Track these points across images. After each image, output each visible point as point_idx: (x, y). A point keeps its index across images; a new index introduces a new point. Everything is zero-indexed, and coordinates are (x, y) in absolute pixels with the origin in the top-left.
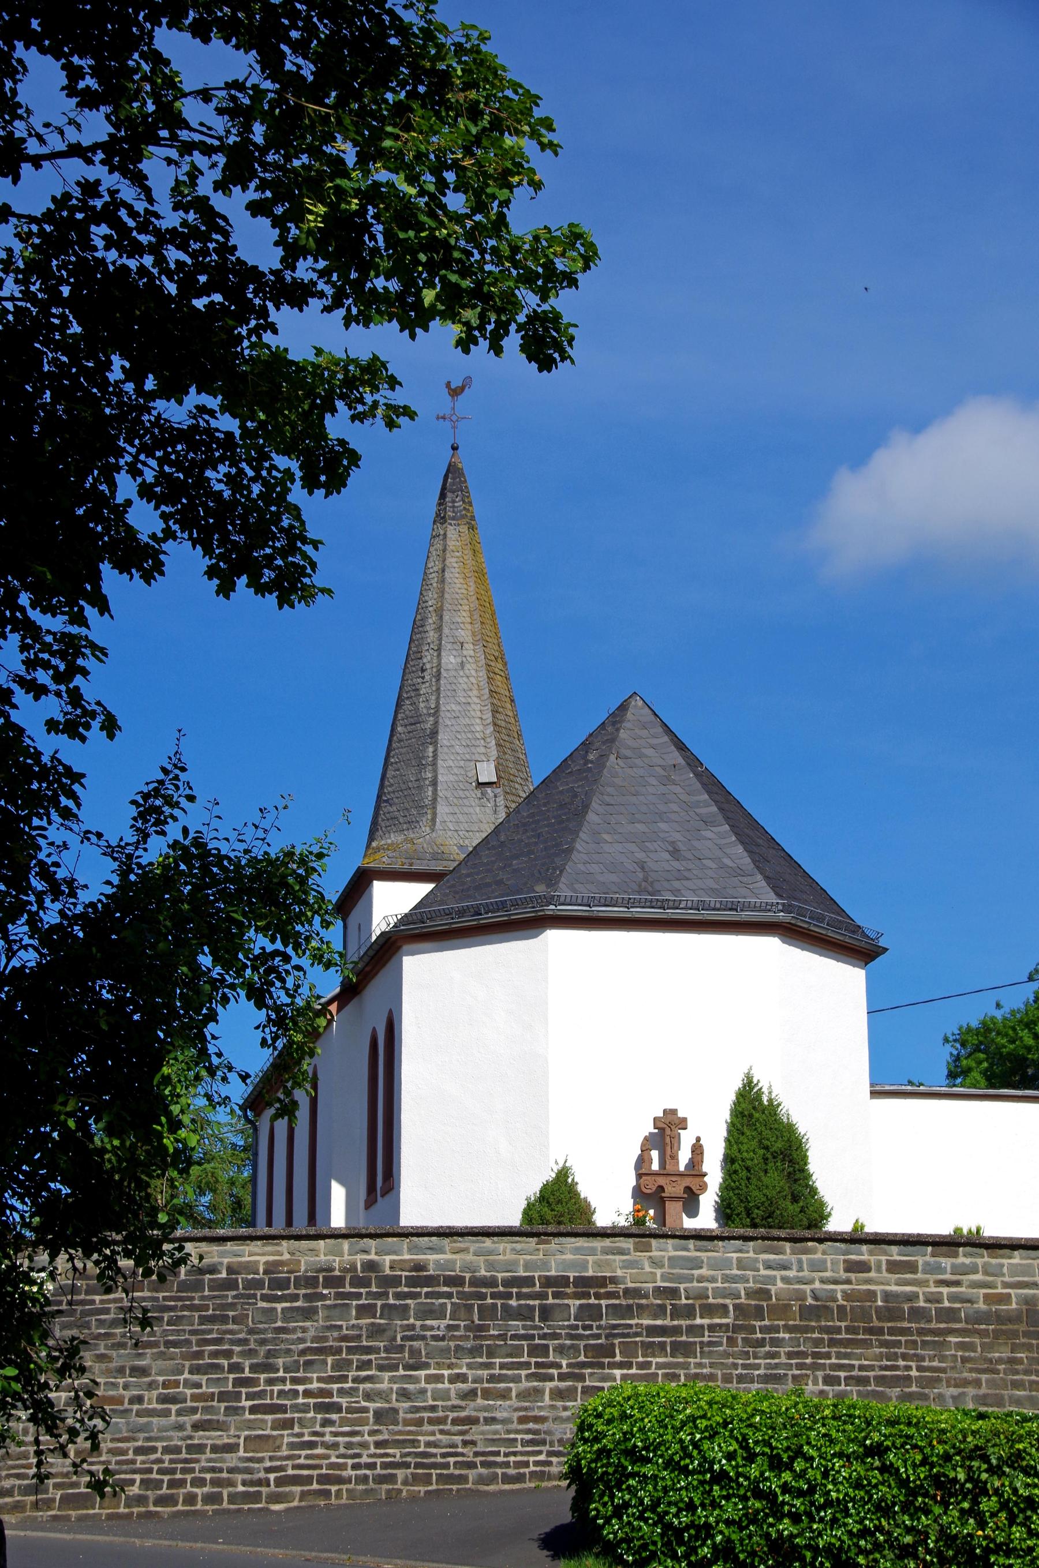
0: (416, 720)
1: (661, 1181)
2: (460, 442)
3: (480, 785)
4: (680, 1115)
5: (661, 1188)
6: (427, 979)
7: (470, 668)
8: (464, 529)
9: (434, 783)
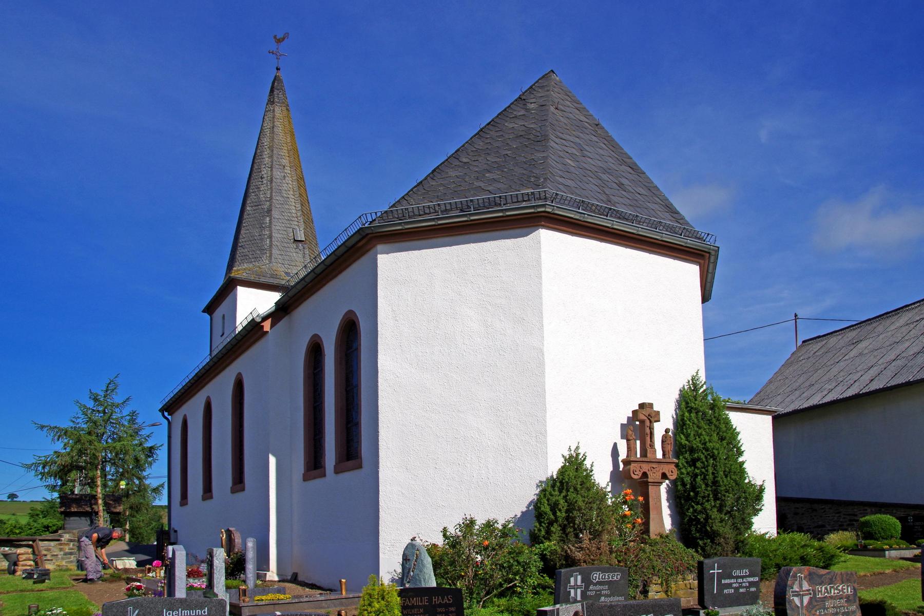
0: (258, 204)
1: (646, 467)
2: (280, 66)
3: (295, 241)
4: (655, 409)
5: (645, 475)
6: (406, 282)
7: (288, 180)
8: (284, 109)
9: (270, 237)
